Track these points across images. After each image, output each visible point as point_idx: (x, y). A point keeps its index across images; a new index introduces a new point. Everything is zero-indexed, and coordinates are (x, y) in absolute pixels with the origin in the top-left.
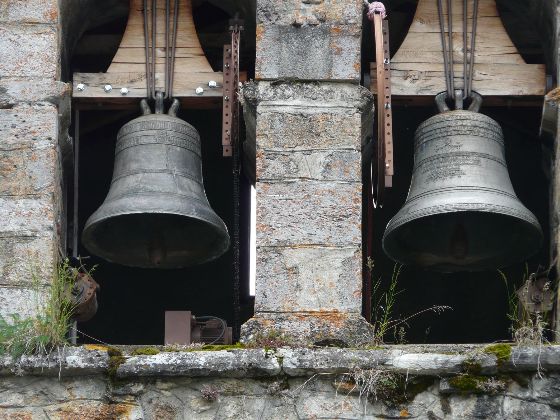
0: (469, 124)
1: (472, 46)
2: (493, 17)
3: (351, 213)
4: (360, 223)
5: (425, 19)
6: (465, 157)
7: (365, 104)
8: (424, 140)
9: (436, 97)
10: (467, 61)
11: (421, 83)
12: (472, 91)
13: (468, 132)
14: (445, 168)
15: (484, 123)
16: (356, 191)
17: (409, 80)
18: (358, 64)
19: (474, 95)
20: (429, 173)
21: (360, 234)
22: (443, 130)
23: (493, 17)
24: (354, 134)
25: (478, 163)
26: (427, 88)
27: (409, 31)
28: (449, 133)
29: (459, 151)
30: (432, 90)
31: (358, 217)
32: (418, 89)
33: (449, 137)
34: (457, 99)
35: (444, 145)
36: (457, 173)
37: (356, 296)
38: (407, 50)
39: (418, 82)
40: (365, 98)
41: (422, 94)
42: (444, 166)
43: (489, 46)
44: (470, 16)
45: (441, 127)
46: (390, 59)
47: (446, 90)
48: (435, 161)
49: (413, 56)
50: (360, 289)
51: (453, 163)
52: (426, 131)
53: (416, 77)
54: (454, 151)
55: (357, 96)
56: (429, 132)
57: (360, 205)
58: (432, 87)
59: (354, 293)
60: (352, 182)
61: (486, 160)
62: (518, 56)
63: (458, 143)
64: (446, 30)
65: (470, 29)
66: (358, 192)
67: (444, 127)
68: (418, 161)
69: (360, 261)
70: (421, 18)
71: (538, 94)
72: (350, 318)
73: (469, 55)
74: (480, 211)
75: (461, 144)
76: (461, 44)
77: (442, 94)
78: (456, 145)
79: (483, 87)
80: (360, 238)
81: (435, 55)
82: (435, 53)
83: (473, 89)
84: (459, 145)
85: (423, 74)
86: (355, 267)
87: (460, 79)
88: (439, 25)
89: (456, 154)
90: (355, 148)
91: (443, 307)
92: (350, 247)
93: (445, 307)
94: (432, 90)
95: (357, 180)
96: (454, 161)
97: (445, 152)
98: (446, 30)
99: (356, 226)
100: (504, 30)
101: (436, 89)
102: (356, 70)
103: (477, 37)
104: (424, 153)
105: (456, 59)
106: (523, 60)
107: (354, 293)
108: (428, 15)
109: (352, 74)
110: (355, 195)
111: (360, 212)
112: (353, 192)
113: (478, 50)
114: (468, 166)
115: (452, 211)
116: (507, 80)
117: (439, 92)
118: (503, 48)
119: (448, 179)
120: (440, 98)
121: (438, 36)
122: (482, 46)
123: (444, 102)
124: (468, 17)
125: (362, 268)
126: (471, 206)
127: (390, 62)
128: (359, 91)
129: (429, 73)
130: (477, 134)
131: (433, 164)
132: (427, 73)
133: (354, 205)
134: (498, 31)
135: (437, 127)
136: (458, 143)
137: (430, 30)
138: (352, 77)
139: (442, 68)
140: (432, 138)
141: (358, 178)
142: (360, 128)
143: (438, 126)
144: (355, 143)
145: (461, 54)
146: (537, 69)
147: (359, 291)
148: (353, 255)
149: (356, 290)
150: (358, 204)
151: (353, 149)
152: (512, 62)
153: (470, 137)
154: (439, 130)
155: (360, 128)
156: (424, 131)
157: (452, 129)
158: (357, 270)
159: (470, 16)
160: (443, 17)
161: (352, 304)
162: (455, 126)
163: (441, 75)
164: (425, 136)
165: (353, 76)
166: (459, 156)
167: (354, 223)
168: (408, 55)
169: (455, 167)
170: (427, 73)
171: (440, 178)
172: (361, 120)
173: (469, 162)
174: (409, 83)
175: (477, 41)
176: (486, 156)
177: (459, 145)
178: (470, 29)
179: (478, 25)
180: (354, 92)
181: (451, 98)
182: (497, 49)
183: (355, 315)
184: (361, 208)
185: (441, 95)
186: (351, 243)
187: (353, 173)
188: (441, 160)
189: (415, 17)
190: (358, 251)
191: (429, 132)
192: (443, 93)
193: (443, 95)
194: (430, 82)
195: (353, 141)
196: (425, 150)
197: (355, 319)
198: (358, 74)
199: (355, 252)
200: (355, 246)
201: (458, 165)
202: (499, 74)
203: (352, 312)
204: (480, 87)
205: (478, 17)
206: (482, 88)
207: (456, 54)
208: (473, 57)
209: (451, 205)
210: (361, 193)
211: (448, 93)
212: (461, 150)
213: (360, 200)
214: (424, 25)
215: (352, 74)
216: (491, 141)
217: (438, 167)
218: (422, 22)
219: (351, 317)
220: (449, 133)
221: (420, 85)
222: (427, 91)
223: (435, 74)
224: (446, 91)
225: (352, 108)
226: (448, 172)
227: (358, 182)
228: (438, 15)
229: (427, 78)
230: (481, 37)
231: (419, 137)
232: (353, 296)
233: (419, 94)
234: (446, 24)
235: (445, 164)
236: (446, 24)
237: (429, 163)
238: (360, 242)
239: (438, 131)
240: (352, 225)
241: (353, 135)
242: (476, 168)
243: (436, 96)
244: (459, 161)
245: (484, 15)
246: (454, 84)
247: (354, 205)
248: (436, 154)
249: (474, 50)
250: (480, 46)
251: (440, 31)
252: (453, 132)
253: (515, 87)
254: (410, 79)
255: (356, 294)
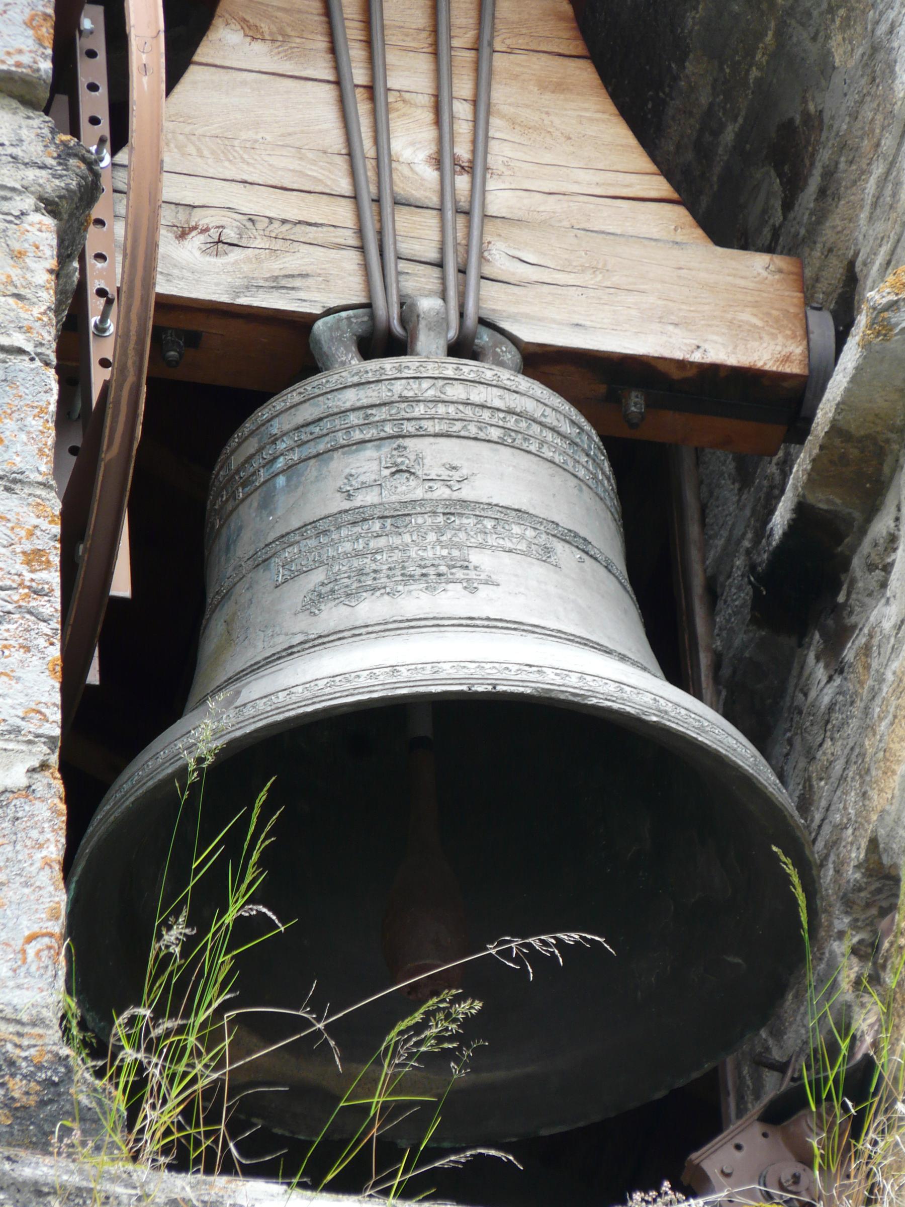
0: (498, 403)
1: (474, 152)
2: (560, 55)
3: (10, 607)
4: (55, 652)
5: (265, 27)
6: (489, 524)
7: (74, 185)
8: (280, 463)
9: (319, 325)
10: (456, 202)
11: (248, 260)
12: (482, 322)
13: (495, 433)
14: (397, 555)
15: (562, 418)
16: (36, 521)
17: (196, 241)
18: (46, 16)
19: (486, 338)
20: (319, 576)
21: (57, 698)
22: (380, 414)
23: (560, 55)
24: (22, 292)
25: (546, 555)
26: (277, 284)
27: (196, 58)
28: (409, 427)
29: (456, 495)
30: (302, 295)
31: (44, 627)
32: (238, 282)
33: (407, 442)
34: (422, 325)
35: (387, 472)
36: (460, 574)
37: (38, 954)
38: (188, 129)
39: (236, 255)
40: (73, 162)
41: (256, 304)
42: (392, 549)
43: (548, 158)
44: (462, 38)
45: (365, 402)
46: (113, 153)
47: (360, 299)
48: (344, 532)
49: (213, 152)
50: (58, 927)
51: (432, 537)
52: (286, 427)
53: (230, 235)
54: (435, 495)
55: (34, 149)
56: (308, 425)
57: (53, 578)
58: (297, 283)
59: (31, 939)
60: (15, 481)
61: (579, 554)
62: (680, 214)
63: (454, 468)
64: (360, 76)
65: (463, 86)
66: (44, 524)
67: (384, 404)
68: (244, 548)
69: (54, 810)
70: (244, 20)
71: (771, 366)
72: (9, 1047)
73: (462, 182)
74: (594, 701)
75: (464, 472)
76: (428, 134)
77: (344, 314)
78: (445, 474)
79: (523, 309)
80: (56, 715)
81: (314, 162)
82: (310, 155)
83: (485, 314)
84: (456, 475)
85: (260, 226)
86: (34, 834)
87: (423, 267)
88: (329, 56)
89: (447, 506)
90: (29, 347)
91: (560, 944)
92: (11, 746)
93: (571, 937)
94: (302, 295)
95: (40, 479)
96: (440, 531)
97: (394, 498)
98: (360, 76)
99: (35, 661)
100: (612, 109)
101: (319, 290)
102: (40, 41)
103: (495, 121)
104: (280, 512)
105: (404, 187)
106: (699, 232)
107: (31, 939)
108: (279, 14)
109: (20, 52)
110: (31, 534)
111: (52, 606)
112: (18, 524)
113: (502, 168)
114: (506, 558)
115: (465, 688)
116: (631, 299)
117: (332, 304)
118: (609, 174)
119: (415, 593)
120: (337, 327)
121: (327, 93)
122: (519, 155)
123: (354, 349)
124: (455, 43)
125: (63, 840)
126: (553, 676)
127: (114, 165)
128: (46, 131)
129: (287, 226)
130: (533, 448)
131: (333, 544)
132: (276, 224)
133: (28, 576)
134: (586, 110)
135: (348, 405)
136: (454, 468)
137: (287, 67)
138: (18, 64)
139: (344, 213)
140: (321, 447)
141: (43, 468)
142: (51, 271)
143: (350, 398)
144: (29, 330)
145: (430, 175)
146: (765, 274)
147: (51, 935)
148: (23, 781)
149: (36, 928)
150: (43, 575)
151: (20, 351)
152: (654, 231)
153: (505, 452)
154: (361, 414)
155: (51, 271)
156: (275, 428)
157: (420, 410)
158: (41, 846)
159: (462, 38)
160: (344, 27)
161: (19, 987)
162: (436, 401)
163: (341, 241)
164: (281, 446)
165: (26, 59)
166: (461, 515)
167: (27, 649)
168: (191, 149)
169: (445, 552)
170: (276, 224)
171: (375, 589)
172: (55, 242)
173: (508, 544)
174: (197, 253)
175: (497, 135)
176: (571, 538)
177: (456, 475)
178: (463, 86)
179: (496, 78)
180: (24, 133)
181: (389, 331)
182: (583, 175)
183: (31, 1036)
184: (58, 593)
185: (340, 320)
186: (17, 731)
187: (19, 448)
188: (376, 526)
189: (219, 10)
190: (44, 766)
191: (308, 425)
192: (351, 312)
193: (349, 318)
194: (292, 262)
195: (18, 318)
196: (282, 502)
197: (32, 1051)
198: (45, 57)
199: (33, 770)
200: (30, 742)
201: (459, 546)
202: (595, 270)
203: (19, 1022)
204: (513, 309)
205: (498, 46)
206: (527, 316)
207: (406, 171)
208: (478, 189)
209: (460, 664)
210: (57, 529)
211: (372, 317)
212: (467, 493)
213: (56, 560)
214: (258, 46)
215: (20, 52)
216: (587, 494)
217: (358, 555)
218: (253, 33)
219: (16, 1039)
220: (409, 427)
221: (245, 268)
222: (276, 294)
223: (312, 234)
224: (368, 306)
225: (13, 189)
226: (412, 569)
227: (45, 485)
228: (324, 19)
229: (278, 245)
230: (513, 122)
231: (251, 457)
232: (24, 951)
233: (243, 301)
234: (356, 53)
235: (396, 541)
236: (356, 53)
237: (312, 543)
238: (57, 732)
239: (354, 419)
240: (20, 654)
241: (18, 296)
242: (539, 570)
243: (317, 317)
244: (462, 535)
245: (521, 42)
246: (398, 282)
247: (28, 576)
248: (346, 505)
249: (486, 169)
250: (510, 154)
251: (331, 78)
252: (425, 424)
253: (671, 328)
254: (202, 238)
255: (32, 949)
